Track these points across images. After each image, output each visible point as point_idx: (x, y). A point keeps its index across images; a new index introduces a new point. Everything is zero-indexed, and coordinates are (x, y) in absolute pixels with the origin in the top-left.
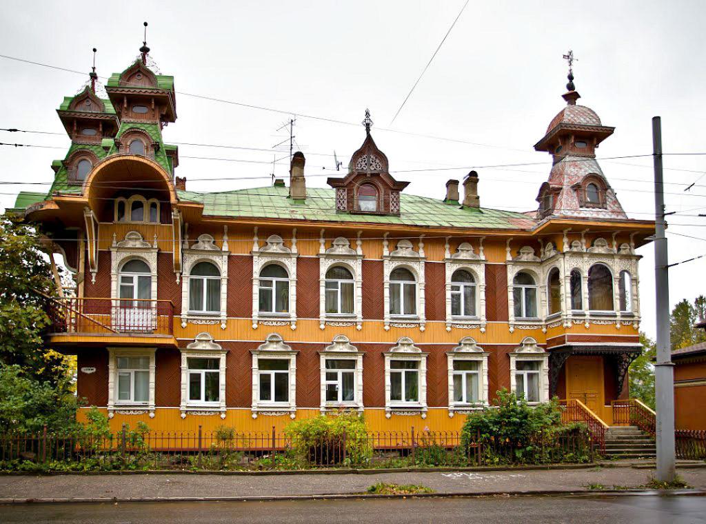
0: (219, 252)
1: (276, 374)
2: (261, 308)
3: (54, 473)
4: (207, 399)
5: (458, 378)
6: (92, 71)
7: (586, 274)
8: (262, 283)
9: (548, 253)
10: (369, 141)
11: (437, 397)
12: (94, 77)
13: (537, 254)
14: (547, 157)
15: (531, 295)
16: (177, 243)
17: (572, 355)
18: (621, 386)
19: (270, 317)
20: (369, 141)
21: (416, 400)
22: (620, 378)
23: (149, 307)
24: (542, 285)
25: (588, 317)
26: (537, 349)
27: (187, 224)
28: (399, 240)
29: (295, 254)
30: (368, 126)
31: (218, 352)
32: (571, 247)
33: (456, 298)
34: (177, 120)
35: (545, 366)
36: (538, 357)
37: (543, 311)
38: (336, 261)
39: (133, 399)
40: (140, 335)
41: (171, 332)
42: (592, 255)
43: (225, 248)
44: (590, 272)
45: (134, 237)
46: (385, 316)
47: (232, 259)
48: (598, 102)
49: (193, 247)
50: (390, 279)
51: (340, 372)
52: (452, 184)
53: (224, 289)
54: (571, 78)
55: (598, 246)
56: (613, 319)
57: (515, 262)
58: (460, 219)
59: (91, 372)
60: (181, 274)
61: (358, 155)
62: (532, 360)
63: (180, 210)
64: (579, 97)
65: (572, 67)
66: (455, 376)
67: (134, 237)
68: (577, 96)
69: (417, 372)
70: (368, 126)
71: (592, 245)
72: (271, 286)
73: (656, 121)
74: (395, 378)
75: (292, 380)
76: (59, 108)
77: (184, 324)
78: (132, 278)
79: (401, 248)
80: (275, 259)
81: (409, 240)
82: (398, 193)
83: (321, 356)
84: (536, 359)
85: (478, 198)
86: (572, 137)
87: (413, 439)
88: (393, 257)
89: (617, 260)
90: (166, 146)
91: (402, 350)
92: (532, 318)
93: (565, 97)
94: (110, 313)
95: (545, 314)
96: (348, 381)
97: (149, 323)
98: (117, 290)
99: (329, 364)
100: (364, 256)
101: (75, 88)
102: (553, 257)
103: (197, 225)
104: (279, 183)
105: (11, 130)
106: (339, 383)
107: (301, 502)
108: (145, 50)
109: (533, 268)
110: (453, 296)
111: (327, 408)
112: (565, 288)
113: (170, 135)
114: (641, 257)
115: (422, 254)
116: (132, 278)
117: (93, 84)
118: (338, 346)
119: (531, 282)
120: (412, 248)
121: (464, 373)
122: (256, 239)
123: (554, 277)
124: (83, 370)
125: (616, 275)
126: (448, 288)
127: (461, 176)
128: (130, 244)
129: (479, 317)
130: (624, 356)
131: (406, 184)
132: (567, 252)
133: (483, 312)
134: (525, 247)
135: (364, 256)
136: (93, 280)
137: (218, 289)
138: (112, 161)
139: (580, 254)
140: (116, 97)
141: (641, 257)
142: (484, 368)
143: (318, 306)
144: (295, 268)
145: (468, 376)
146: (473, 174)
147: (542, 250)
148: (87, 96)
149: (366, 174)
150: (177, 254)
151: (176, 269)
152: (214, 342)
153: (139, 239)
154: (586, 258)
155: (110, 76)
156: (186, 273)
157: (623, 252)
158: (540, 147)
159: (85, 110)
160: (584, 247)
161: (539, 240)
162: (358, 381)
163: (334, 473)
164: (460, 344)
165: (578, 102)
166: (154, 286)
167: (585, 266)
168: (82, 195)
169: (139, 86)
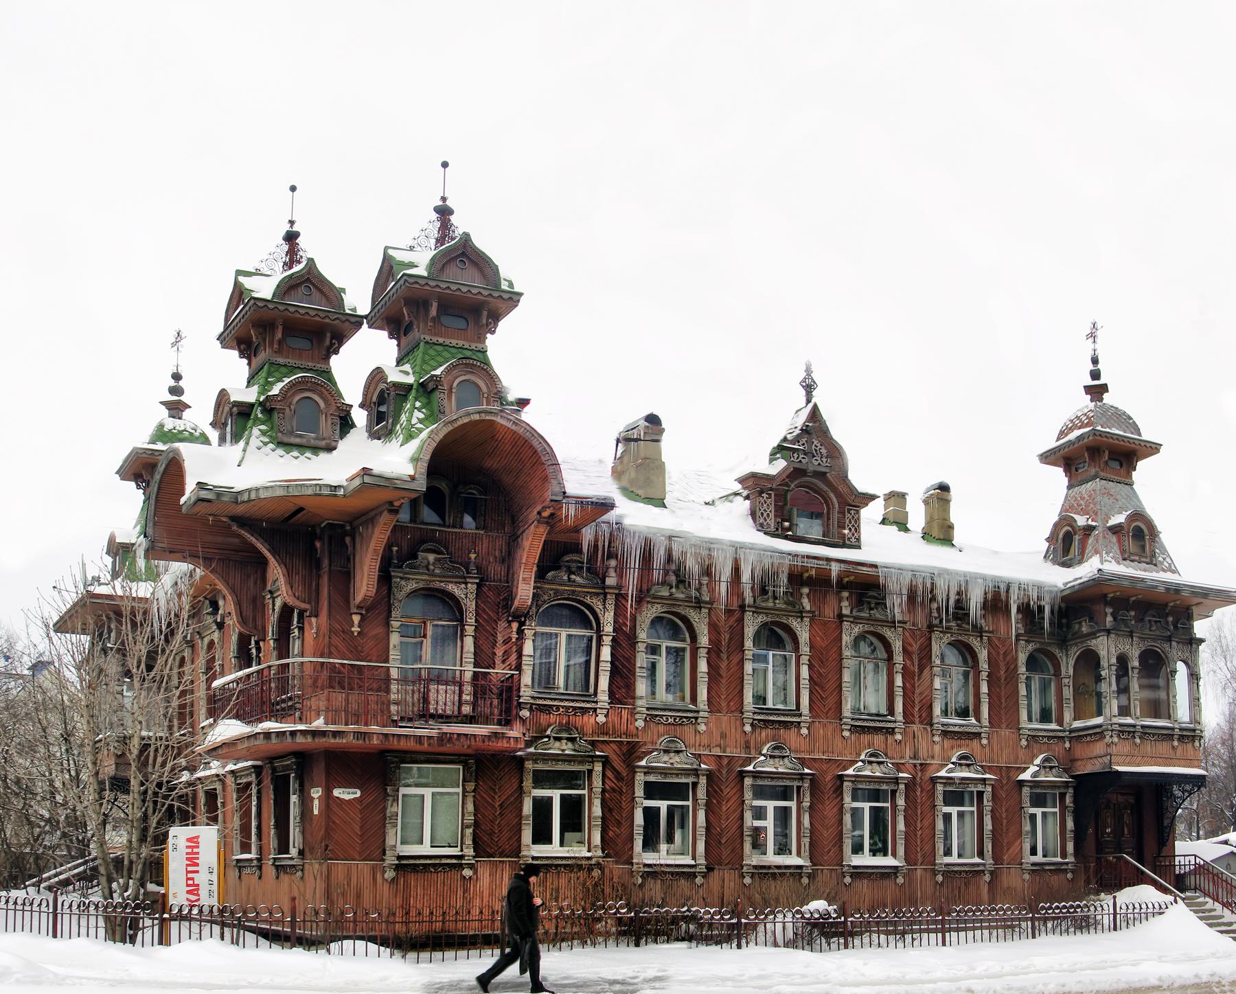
1: (562, 796)
7: (1136, 663)
14: (1058, 476)
20: (815, 414)
39: (429, 844)
48: (1138, 401)
51: (771, 805)
54: (1095, 361)
59: (352, 796)
65: (1092, 346)
68: (1104, 388)
86: (1101, 454)
87: (293, 922)
93: (1088, 389)
94: (388, 691)
106: (769, 823)
124: (337, 793)
158: (1048, 458)
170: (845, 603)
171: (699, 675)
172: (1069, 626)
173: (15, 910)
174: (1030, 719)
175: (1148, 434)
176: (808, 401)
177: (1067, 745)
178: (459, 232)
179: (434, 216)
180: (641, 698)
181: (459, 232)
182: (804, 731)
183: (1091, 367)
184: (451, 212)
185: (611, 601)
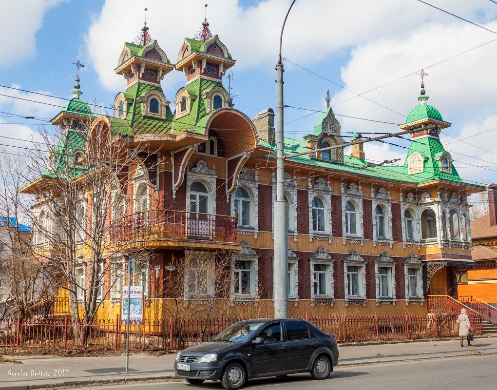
1: (242, 272)
3: (386, 343)
20: (331, 114)
24: (417, 219)
46: (310, 232)
73: (328, 92)
78: (195, 196)
92: (246, 226)
105: (408, 140)
107: (481, 344)
116: (195, 196)
136: (174, 196)
163: (351, 345)
170: (342, 188)
171: (231, 210)
172: (419, 199)
173: (363, 322)
174: (347, 231)
176: (328, 107)
178: (214, 35)
179: (202, 26)
181: (214, 35)
182: (391, 247)
184: (208, 25)
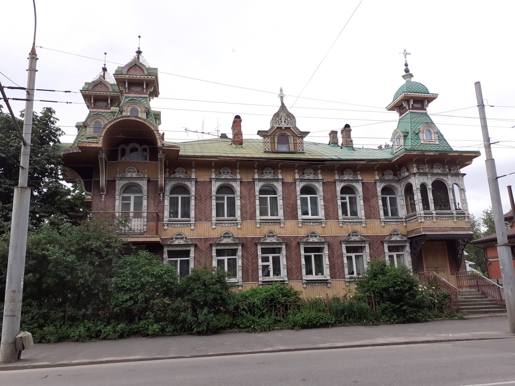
0: (190, 179)
2: (218, 215)
4: (316, 274)
5: (349, 259)
6: (103, 66)
7: (430, 187)
8: (217, 199)
9: (403, 174)
10: (283, 106)
11: (336, 272)
12: (105, 70)
13: (395, 175)
14: (395, 115)
15: (393, 202)
16: (161, 174)
17: (427, 241)
18: (461, 261)
19: (224, 221)
20: (283, 106)
21: (322, 275)
22: (459, 256)
23: (141, 217)
24: (400, 194)
25: (434, 215)
26: (278, 240)
27: (167, 161)
28: (305, 169)
29: (238, 179)
30: (282, 98)
31: (236, 244)
32: (418, 169)
33: (344, 205)
34: (159, 96)
35: (408, 249)
36: (402, 243)
37: (402, 212)
38: (346, 184)
40: (135, 236)
41: (157, 233)
42: (433, 174)
43: (193, 176)
44: (433, 184)
45: (131, 170)
47: (334, 184)
48: (425, 78)
49: (172, 176)
50: (341, 194)
51: (271, 256)
52: (333, 133)
53: (193, 203)
54: (406, 65)
55: (436, 168)
56: (451, 216)
57: (381, 181)
58: (344, 154)
60: (164, 194)
61: (277, 115)
62: (313, 246)
63: (164, 151)
64: (413, 76)
65: (405, 59)
66: (306, 257)
67: (131, 170)
69: (322, 255)
70: (282, 98)
71: (432, 168)
72: (224, 200)
74: (308, 259)
75: (239, 263)
76: (81, 89)
77: (166, 227)
79: (307, 173)
80: (226, 183)
81: (312, 168)
82: (302, 139)
83: (301, 245)
84: (401, 245)
85: (352, 141)
86: (413, 102)
88: (302, 179)
89: (449, 177)
90: (153, 112)
91: (176, 242)
95: (404, 214)
96: (276, 261)
97: (142, 227)
98: (119, 206)
99: (264, 251)
100: (283, 179)
101: (93, 76)
102: (407, 176)
103: (175, 161)
104: (224, 136)
106: (270, 263)
108: (139, 52)
109: (393, 184)
110: (342, 203)
111: (263, 282)
112: (418, 196)
113: (155, 104)
114: (465, 174)
115: (238, 176)
117: (104, 74)
118: (269, 238)
119: (314, 193)
120: (274, 173)
121: (353, 255)
122: (213, 170)
123: (409, 189)
125: (449, 187)
126: (339, 198)
127: (339, 127)
128: (129, 175)
129: (360, 217)
130: (460, 241)
131: (308, 133)
132: (417, 173)
133: (363, 214)
134: (387, 171)
135: (197, 179)
137: (189, 204)
138: (118, 120)
139: (426, 174)
140: (120, 81)
141: (465, 174)
142: (367, 251)
143: (255, 212)
144: (146, 187)
145: (356, 257)
146: (347, 126)
147: (398, 172)
148: (100, 83)
149: (282, 128)
150: (161, 181)
151: (160, 191)
152: (186, 239)
153: (135, 172)
154: (429, 176)
155: (117, 68)
156: (167, 193)
157: (453, 172)
159: (100, 92)
160: (427, 169)
161: (396, 166)
162: (283, 262)
164: (308, 236)
165: (413, 79)
166: (145, 203)
167: (429, 182)
168: (97, 143)
169: (137, 75)
175: (432, 90)
177: (405, 224)
180: (166, 217)
183: (405, 67)
185: (193, 183)
